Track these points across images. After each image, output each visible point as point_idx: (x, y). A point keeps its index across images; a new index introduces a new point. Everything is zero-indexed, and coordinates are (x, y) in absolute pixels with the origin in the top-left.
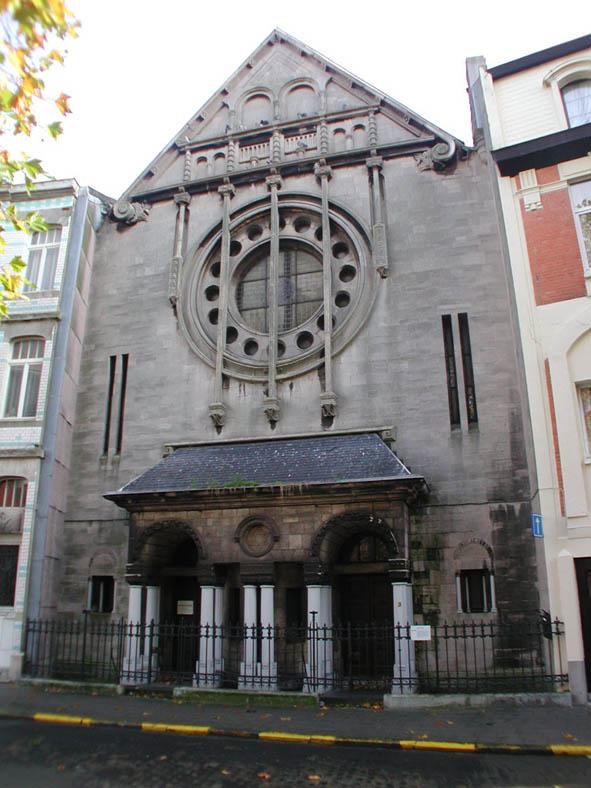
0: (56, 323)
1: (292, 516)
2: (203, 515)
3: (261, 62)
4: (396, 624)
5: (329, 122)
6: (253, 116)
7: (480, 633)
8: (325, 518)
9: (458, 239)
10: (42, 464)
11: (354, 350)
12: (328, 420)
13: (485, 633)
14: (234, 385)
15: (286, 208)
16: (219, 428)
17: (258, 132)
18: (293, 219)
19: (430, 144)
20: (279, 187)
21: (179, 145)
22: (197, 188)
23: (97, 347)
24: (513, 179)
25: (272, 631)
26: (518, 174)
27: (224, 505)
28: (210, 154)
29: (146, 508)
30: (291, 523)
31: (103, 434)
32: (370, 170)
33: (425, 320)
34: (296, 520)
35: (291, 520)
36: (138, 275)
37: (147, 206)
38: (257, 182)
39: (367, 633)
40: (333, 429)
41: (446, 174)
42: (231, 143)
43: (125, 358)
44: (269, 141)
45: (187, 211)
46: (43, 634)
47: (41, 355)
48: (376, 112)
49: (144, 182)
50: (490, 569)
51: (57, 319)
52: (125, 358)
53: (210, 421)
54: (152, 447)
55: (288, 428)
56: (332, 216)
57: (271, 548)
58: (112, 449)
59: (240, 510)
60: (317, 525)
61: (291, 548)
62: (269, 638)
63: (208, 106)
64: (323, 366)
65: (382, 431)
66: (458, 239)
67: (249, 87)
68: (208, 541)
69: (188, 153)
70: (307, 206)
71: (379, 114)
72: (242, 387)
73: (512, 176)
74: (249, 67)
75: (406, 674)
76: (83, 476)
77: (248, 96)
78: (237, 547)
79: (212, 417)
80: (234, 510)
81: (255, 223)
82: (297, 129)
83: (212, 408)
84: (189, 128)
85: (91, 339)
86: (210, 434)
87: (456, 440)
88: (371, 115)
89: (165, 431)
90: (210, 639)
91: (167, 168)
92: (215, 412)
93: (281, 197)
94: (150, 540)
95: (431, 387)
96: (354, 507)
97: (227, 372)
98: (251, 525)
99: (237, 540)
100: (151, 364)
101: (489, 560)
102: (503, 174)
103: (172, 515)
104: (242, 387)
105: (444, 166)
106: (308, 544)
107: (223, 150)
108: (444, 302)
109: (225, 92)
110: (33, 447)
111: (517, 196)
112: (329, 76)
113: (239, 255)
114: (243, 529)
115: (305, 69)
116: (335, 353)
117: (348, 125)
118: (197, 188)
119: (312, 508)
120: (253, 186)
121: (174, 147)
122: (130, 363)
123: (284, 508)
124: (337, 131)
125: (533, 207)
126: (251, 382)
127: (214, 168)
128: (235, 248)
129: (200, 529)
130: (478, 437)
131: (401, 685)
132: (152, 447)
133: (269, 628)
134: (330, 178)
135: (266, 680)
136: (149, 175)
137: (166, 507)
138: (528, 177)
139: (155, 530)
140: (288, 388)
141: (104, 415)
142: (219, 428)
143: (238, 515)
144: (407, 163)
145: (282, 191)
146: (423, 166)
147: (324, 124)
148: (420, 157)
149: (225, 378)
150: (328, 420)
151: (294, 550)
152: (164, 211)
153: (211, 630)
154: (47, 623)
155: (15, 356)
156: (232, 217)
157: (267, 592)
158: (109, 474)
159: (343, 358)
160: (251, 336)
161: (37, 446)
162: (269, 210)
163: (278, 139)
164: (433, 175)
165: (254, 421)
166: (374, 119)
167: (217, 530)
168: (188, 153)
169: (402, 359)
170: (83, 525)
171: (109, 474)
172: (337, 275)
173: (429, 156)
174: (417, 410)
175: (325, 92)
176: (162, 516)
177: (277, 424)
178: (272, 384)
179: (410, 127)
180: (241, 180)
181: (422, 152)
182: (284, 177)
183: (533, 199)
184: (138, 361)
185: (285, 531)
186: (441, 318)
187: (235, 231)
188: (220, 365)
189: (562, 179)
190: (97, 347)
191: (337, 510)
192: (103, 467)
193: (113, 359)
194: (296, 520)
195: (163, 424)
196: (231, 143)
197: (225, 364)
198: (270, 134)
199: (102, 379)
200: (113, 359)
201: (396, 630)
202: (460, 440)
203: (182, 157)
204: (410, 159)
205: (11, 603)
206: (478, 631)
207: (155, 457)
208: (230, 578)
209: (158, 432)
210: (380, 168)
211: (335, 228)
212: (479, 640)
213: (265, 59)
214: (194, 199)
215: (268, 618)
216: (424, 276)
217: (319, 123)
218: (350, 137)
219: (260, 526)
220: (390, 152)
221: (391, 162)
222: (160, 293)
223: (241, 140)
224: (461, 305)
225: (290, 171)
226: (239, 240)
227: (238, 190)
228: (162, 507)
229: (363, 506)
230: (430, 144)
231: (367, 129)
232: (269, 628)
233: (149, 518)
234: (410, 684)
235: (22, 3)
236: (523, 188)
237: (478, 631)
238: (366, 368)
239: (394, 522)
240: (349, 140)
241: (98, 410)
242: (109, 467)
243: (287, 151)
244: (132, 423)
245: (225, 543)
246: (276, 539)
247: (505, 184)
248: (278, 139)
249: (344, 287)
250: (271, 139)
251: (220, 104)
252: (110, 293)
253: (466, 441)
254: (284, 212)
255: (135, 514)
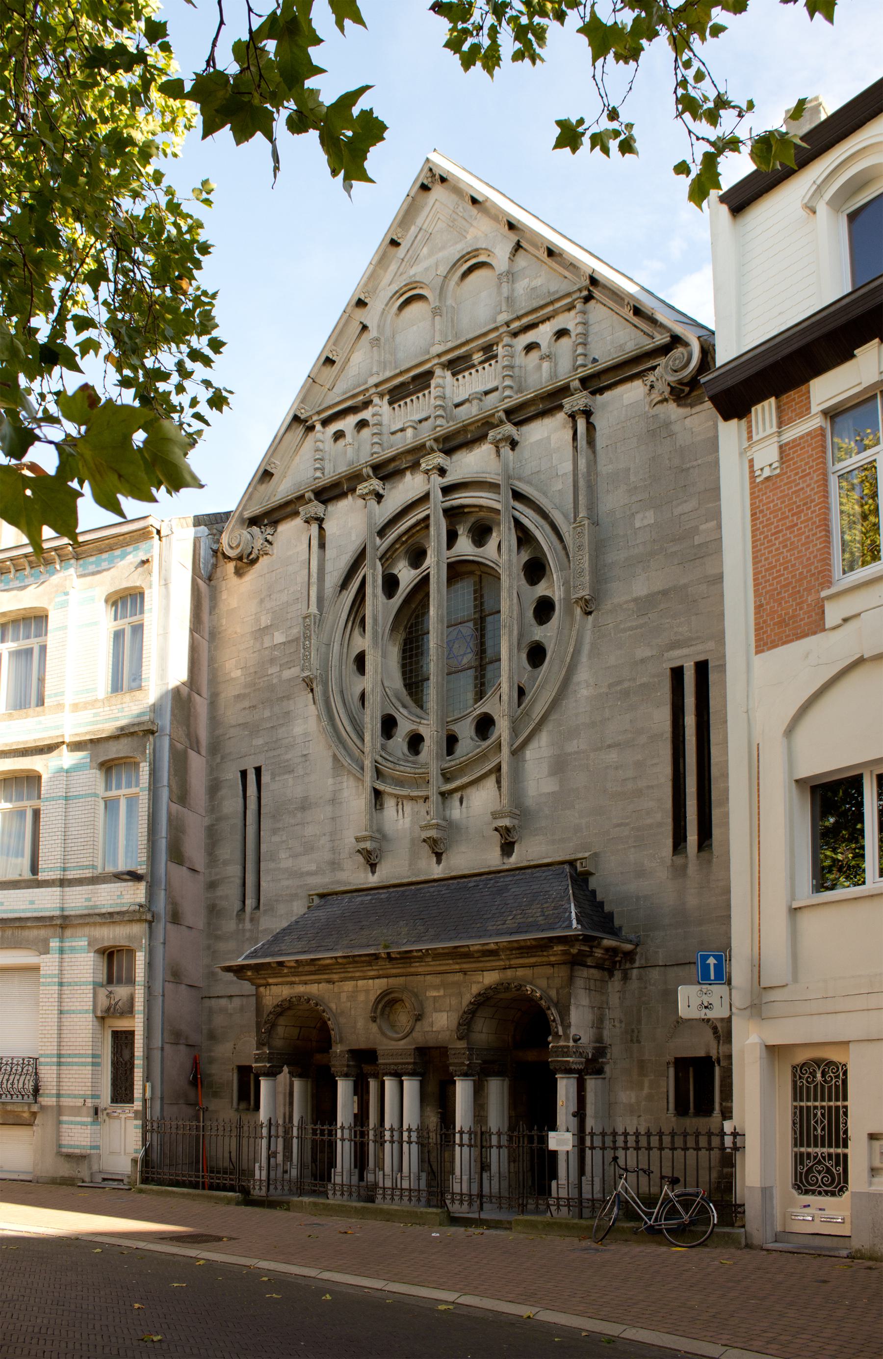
0: (151, 738)
1: (436, 988)
2: (336, 988)
3: (413, 230)
4: (458, 1129)
5: (515, 335)
6: (417, 337)
7: (634, 1145)
8: (475, 989)
9: (703, 527)
10: (150, 928)
11: (543, 739)
12: (507, 848)
13: (688, 1146)
14: (390, 804)
15: (453, 508)
16: (373, 867)
17: (412, 373)
18: (469, 525)
19: (664, 350)
20: (442, 472)
21: (302, 417)
22: (328, 494)
23: (223, 758)
24: (744, 422)
25: (395, 1133)
26: (750, 412)
27: (358, 974)
28: (347, 424)
29: (271, 981)
30: (435, 997)
31: (238, 881)
32: (572, 416)
33: (645, 680)
34: (441, 993)
35: (435, 994)
36: (266, 645)
37: (269, 530)
38: (415, 466)
39: (326, 1132)
40: (514, 860)
41: (692, 406)
42: (376, 400)
43: (258, 770)
44: (429, 386)
45: (321, 528)
46: (655, 1153)
47: (137, 785)
48: (588, 299)
49: (262, 488)
50: (714, 1057)
51: (152, 732)
52: (258, 770)
53: (360, 859)
54: (294, 897)
55: (465, 859)
56: (517, 514)
57: (412, 1030)
58: (250, 902)
59: (377, 981)
60: (467, 998)
61: (434, 1029)
62: (499, 1147)
63: (337, 335)
64: (498, 769)
65: (576, 860)
66: (703, 527)
67: (395, 287)
68: (342, 1020)
69: (318, 427)
70: (413, 521)
71: (593, 302)
72: (400, 806)
73: (740, 417)
74: (394, 243)
75: (563, 1194)
76: (218, 938)
77: (466, 266)
78: (374, 1028)
79: (496, 829)
80: (371, 981)
81: (415, 539)
82: (467, 357)
83: (358, 839)
84: (305, 396)
85: (215, 748)
86: (363, 875)
87: (680, 872)
88: (579, 306)
89: (310, 874)
90: (396, 1145)
91: (292, 459)
92: (363, 845)
93: (447, 490)
94: (282, 1021)
95: (648, 787)
96: (509, 973)
97: (381, 787)
98: (387, 1004)
99: (374, 1019)
100: (289, 779)
101: (713, 1043)
102: (726, 418)
103: (301, 989)
104: (400, 806)
105: (687, 389)
106: (454, 1024)
107: (366, 414)
108: (675, 645)
109: (361, 303)
110: (138, 907)
111: (747, 450)
112: (513, 238)
113: (396, 597)
114: (380, 1006)
115: (481, 233)
116: (515, 746)
117: (543, 334)
118: (328, 494)
119: (459, 977)
120: (408, 474)
121: (296, 419)
122: (265, 779)
123: (428, 977)
124: (530, 347)
125: (767, 473)
126: (412, 799)
127: (354, 450)
128: (391, 584)
129: (333, 1006)
130: (709, 862)
131: (558, 1206)
132: (294, 897)
133: (499, 1134)
134: (514, 444)
135: (389, 1192)
136: (266, 475)
137: (293, 979)
138: (765, 412)
139: (285, 1008)
140: (458, 803)
141: (238, 855)
142: (373, 867)
143: (373, 987)
144: (632, 393)
145: (449, 479)
146: (656, 396)
147: (507, 340)
148: (651, 377)
149: (378, 794)
150: (507, 848)
151: (439, 1032)
152: (292, 534)
153: (405, 1138)
154: (661, 1134)
155: (108, 787)
156: (381, 533)
157: (411, 1086)
158: (248, 934)
159: (530, 754)
160: (414, 727)
161: (141, 906)
162: (427, 517)
163: (443, 379)
164: (672, 409)
165: (414, 856)
166: (584, 312)
167: (350, 1004)
168: (318, 427)
169: (609, 746)
170: (223, 1002)
171: (248, 934)
172: (530, 613)
173: (664, 372)
174: (627, 824)
175: (508, 273)
176: (292, 991)
177: (444, 856)
178: (435, 798)
179: (636, 320)
180: (387, 471)
181: (654, 368)
182: (449, 452)
183: (767, 456)
184: (273, 777)
185: (429, 1007)
186: (668, 672)
187: (387, 558)
188: (369, 774)
189: (815, 408)
190: (223, 758)
191: (490, 978)
192: (241, 926)
193: (244, 774)
194: (441, 993)
195: (307, 864)
196: (376, 400)
197: (379, 774)
198: (430, 374)
199: (231, 804)
200: (244, 774)
201: (457, 1136)
202: (685, 867)
203: (311, 436)
204: (638, 383)
205: (131, 1101)
206: (703, 1142)
207: (299, 908)
208: (365, 1065)
209: (302, 875)
210: (587, 413)
211: (525, 537)
212: (691, 1153)
213: (419, 221)
214: (331, 508)
215: (411, 1118)
216: (647, 603)
217: (500, 338)
218: (548, 357)
219: (395, 1001)
220: (598, 381)
221: (608, 395)
222: (295, 671)
223: (391, 391)
224: (700, 647)
225: (453, 443)
226: (395, 572)
227: (387, 486)
228: (288, 979)
229: (520, 972)
230: (664, 350)
231: (573, 334)
232: (499, 1134)
233: (277, 992)
234: (569, 1206)
235: (287, 7)
236: (755, 438)
237: (703, 1142)
238: (559, 766)
239: (558, 993)
240: (546, 365)
241: (229, 850)
242: (248, 925)
243: (457, 400)
244: (272, 865)
245: (360, 1024)
246: (419, 1018)
247: (729, 432)
248: (443, 379)
249: (539, 633)
250: (433, 383)
251: (356, 328)
252: (233, 675)
253: (692, 869)
254: (453, 514)
255: (262, 989)
